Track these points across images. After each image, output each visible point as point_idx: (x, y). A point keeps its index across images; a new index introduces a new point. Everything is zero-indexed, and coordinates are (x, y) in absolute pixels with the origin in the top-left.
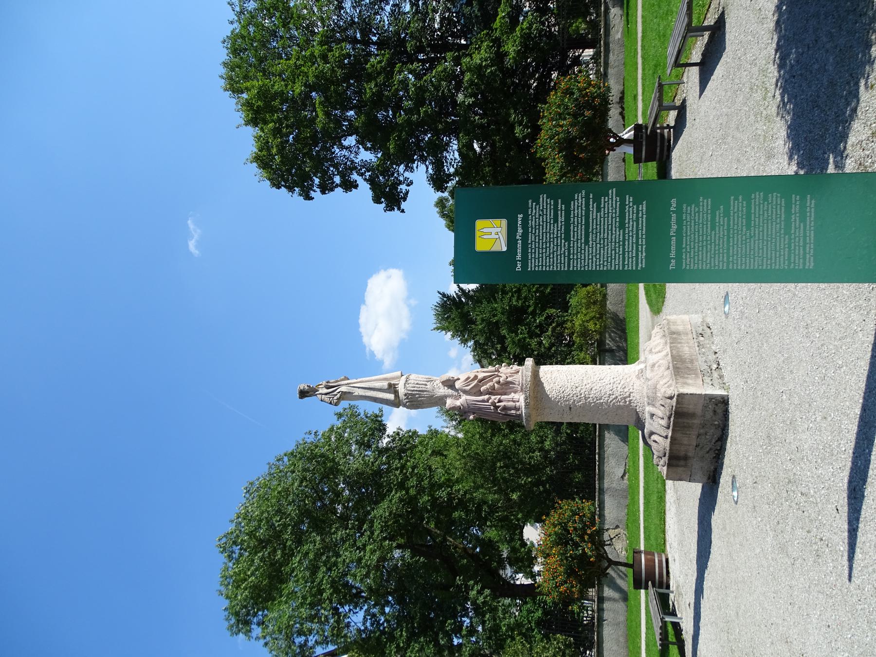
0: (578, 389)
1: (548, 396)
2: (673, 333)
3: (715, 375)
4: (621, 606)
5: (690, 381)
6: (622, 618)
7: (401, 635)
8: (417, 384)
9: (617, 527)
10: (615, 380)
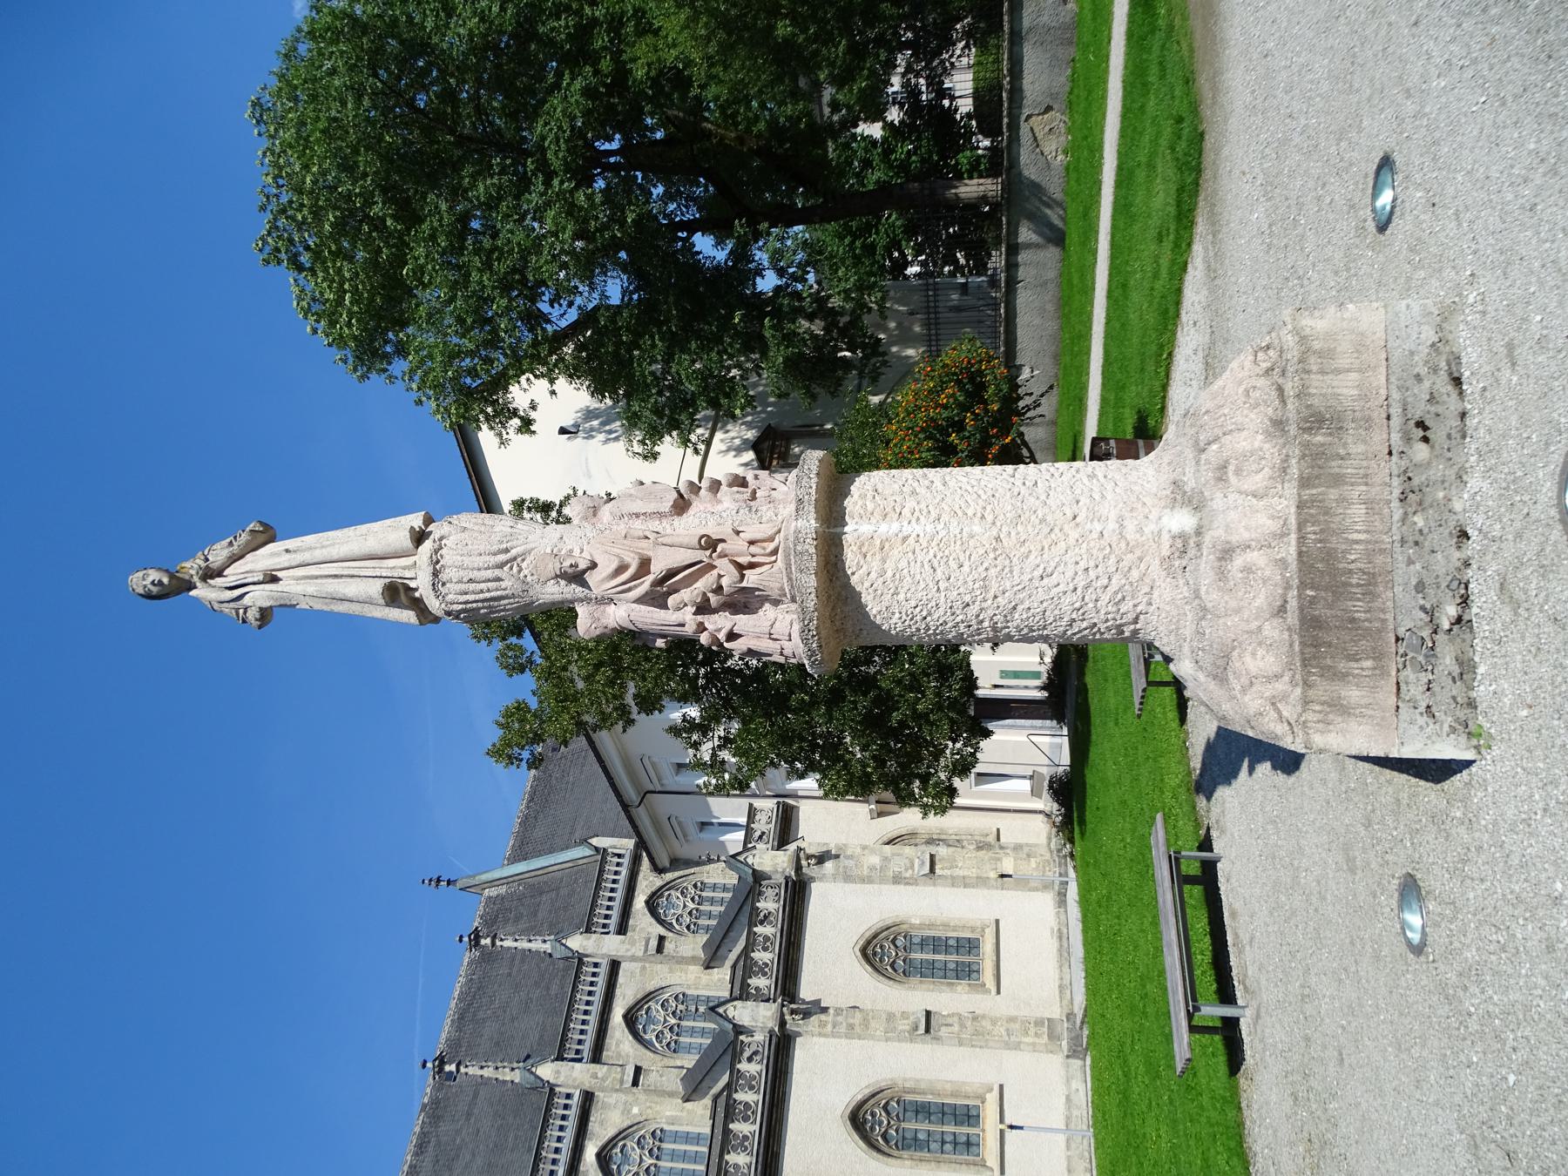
0: (974, 609)
1: (879, 627)
2: (1315, 420)
3: (1447, 661)
4: (1052, 252)
5: (1353, 694)
6: (1051, 274)
7: (654, 346)
8: (470, 581)
9: (1049, 109)
10: (1092, 574)
